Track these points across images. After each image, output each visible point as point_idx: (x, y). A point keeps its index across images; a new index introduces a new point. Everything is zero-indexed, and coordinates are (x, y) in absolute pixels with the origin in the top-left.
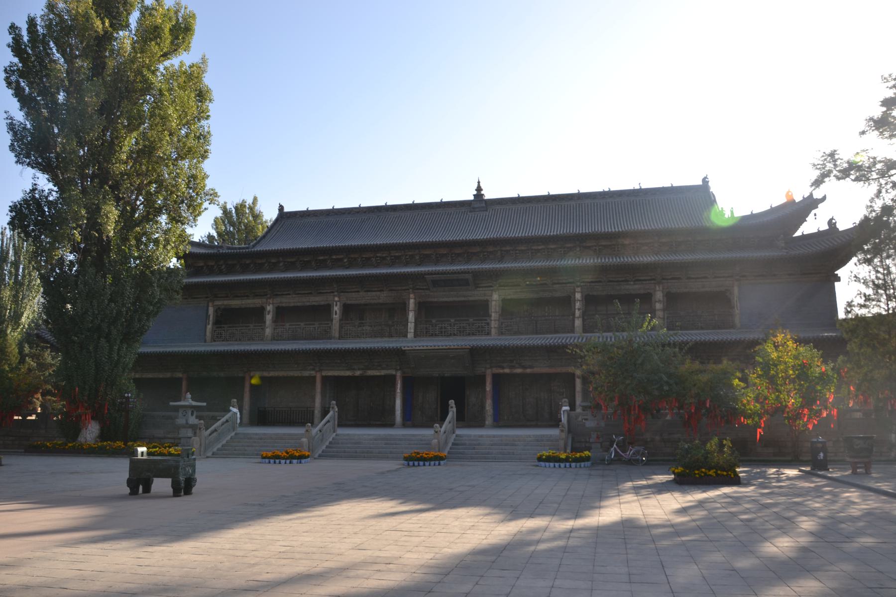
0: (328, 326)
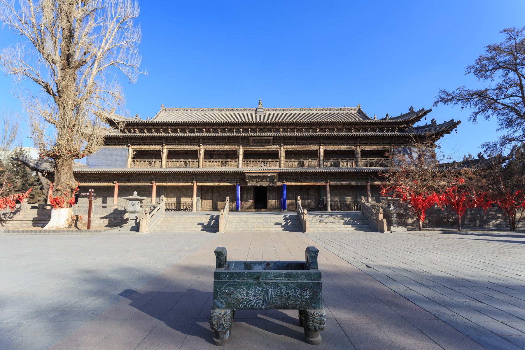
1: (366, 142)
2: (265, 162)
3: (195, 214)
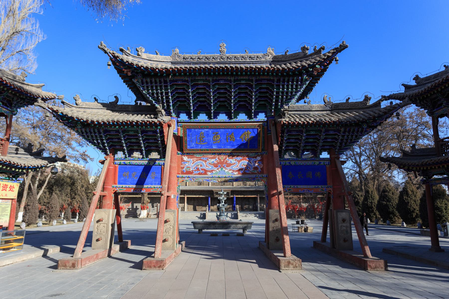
3: (186, 212)
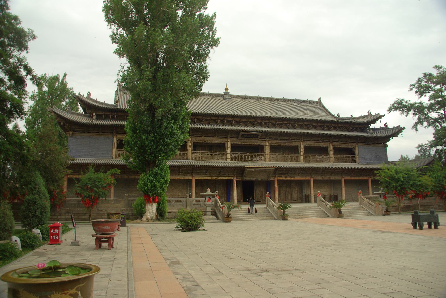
0: (185, 153)
1: (337, 140)
2: (261, 156)
